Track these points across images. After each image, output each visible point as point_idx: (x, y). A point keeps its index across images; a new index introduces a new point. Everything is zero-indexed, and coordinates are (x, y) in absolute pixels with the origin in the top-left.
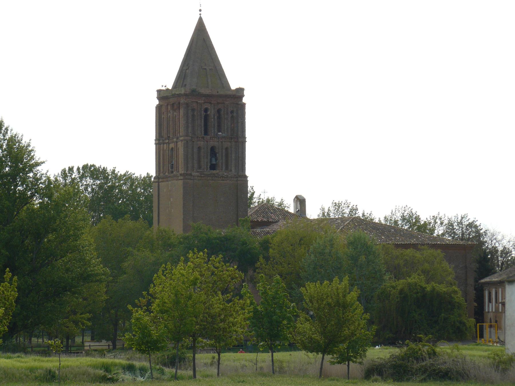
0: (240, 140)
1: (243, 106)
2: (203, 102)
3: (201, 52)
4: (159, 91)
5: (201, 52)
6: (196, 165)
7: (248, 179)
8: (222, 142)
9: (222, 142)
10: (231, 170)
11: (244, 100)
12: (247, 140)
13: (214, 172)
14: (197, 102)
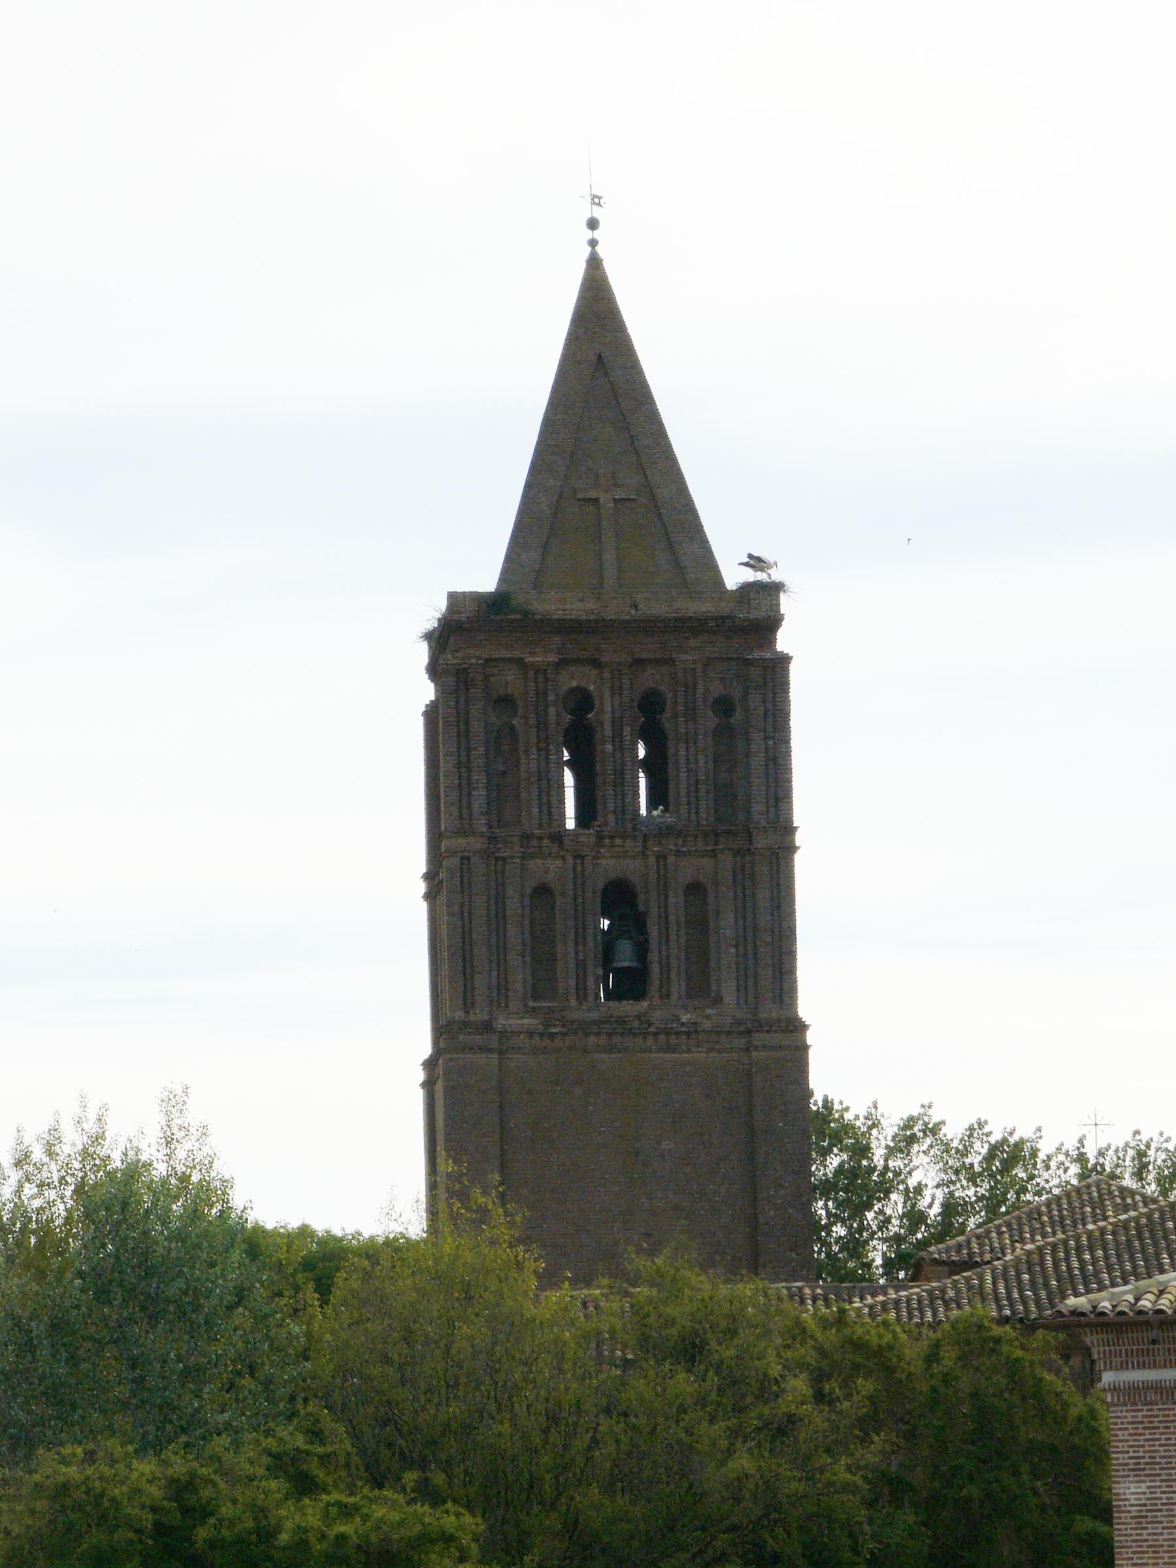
0: (761, 842)
1: (773, 674)
2: (553, 658)
3: (601, 425)
4: (791, 658)
5: (601, 425)
6: (519, 979)
7: (811, 1037)
8: (661, 858)
9: (661, 858)
10: (718, 1000)
11: (784, 641)
12: (799, 839)
13: (627, 1008)
14: (520, 662)
